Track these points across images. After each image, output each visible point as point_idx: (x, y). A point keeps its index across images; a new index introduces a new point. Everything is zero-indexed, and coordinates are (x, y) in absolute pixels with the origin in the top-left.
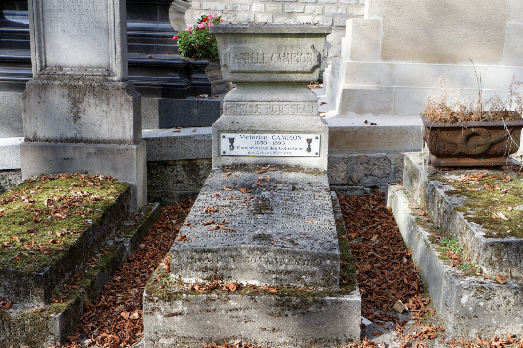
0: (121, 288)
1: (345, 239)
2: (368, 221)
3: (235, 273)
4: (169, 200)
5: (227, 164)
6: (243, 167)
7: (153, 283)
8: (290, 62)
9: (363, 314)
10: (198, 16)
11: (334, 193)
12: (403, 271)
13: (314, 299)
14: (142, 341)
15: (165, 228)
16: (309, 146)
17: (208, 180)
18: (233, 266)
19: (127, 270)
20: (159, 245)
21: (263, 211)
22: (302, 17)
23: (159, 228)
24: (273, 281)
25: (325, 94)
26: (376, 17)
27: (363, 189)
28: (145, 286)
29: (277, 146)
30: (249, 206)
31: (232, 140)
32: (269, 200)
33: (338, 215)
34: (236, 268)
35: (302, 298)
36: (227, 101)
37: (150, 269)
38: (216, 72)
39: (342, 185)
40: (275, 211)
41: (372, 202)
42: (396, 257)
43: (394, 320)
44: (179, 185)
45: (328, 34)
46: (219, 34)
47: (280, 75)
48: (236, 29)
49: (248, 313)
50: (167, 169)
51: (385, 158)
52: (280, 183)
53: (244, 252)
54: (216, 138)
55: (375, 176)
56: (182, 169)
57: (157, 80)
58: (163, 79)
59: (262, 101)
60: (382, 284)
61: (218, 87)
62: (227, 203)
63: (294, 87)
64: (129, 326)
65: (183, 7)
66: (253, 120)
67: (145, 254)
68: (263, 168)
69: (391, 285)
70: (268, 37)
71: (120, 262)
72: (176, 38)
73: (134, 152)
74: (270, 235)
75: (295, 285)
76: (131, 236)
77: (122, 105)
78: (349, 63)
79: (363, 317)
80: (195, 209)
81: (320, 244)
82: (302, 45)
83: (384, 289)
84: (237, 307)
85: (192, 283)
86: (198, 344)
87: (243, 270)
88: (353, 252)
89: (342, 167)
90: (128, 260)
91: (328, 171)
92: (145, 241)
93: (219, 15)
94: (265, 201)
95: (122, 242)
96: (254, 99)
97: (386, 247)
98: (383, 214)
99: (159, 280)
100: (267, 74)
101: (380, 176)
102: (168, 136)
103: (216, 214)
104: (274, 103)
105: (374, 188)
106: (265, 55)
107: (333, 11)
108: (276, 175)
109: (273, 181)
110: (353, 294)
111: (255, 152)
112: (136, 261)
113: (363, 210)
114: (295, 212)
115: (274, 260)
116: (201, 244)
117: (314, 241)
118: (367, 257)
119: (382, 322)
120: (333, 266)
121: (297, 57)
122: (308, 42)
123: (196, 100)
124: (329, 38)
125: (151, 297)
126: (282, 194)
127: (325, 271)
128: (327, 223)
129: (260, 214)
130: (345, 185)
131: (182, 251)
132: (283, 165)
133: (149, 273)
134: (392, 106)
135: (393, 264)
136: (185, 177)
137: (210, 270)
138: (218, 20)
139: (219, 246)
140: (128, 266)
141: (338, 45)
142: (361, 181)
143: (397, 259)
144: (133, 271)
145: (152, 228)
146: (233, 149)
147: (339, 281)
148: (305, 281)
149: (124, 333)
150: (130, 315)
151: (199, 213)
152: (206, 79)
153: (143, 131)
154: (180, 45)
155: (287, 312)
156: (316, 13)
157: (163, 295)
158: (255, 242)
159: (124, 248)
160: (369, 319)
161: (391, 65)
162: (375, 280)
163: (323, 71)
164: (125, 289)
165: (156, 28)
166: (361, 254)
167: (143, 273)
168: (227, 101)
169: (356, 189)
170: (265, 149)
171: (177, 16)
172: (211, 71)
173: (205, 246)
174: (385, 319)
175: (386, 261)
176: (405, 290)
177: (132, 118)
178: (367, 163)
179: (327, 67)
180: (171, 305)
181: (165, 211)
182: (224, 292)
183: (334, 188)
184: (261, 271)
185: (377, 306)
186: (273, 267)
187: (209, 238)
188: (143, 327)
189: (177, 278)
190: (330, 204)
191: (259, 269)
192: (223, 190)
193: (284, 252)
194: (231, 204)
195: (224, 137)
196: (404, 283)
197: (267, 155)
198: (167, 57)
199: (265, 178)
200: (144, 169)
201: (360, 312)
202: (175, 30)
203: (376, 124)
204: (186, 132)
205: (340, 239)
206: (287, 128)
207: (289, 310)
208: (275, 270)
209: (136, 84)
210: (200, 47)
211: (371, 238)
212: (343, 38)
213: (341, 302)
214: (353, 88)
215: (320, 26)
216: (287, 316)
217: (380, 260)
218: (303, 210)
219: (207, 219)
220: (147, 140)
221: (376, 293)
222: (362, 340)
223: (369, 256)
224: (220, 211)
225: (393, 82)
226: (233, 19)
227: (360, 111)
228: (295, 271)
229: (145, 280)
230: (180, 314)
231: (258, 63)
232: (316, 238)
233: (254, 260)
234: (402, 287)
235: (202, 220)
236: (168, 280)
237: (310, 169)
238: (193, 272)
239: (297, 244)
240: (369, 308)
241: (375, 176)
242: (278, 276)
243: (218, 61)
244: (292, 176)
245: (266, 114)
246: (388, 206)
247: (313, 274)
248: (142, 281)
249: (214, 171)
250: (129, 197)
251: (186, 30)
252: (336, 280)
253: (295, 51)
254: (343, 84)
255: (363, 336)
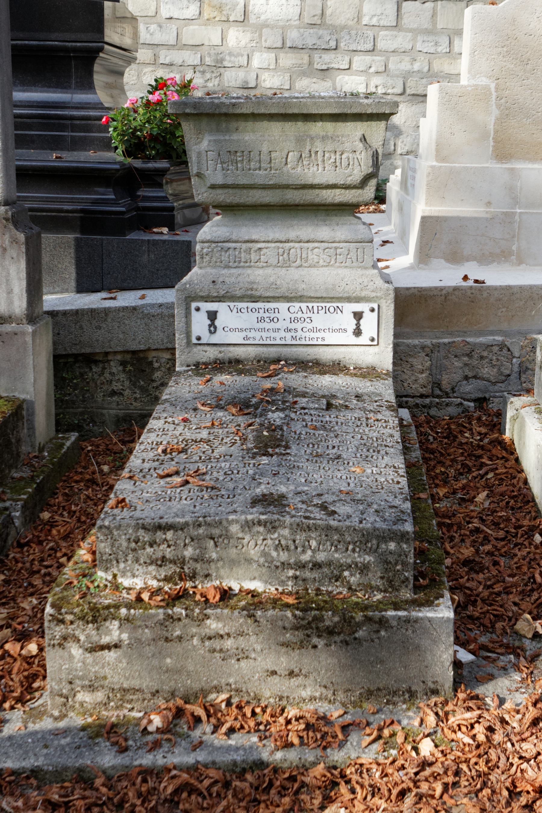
0: (6, 597)
1: (426, 500)
2: (470, 464)
3: (217, 569)
4: (96, 428)
5: (204, 360)
6: (233, 365)
7: (65, 589)
8: (320, 169)
9: (458, 641)
10: (149, 79)
11: (405, 413)
12: (535, 559)
13: (365, 616)
14: (44, 697)
15: (88, 480)
16: (358, 325)
17: (167, 391)
18: (214, 556)
19: (17, 562)
20: (78, 514)
21: (270, 450)
22: (347, 77)
23: (77, 482)
24: (290, 583)
25: (390, 223)
26: (483, 81)
27: (461, 404)
28: (48, 592)
29: (299, 326)
30: (244, 440)
31: (212, 316)
32: (281, 429)
33: (414, 455)
34: (220, 559)
35: (344, 614)
36: (203, 242)
37: (61, 560)
38: (183, 184)
39: (422, 396)
40: (294, 450)
41: (478, 429)
42: (520, 532)
43: (516, 651)
44: (115, 398)
45: (393, 114)
46: (187, 116)
47: (301, 191)
48: (218, 106)
49: (242, 642)
50: (91, 369)
51: (502, 346)
52: (304, 395)
53: (234, 529)
54: (184, 312)
55: (484, 379)
56: (121, 368)
57: (72, 201)
58: (82, 199)
59: (268, 242)
60: (495, 584)
61: (187, 212)
62: (204, 434)
63: (328, 215)
64: (19, 669)
65: (121, 63)
66: (252, 278)
67: (50, 531)
68: (272, 367)
69: (511, 587)
70: (278, 121)
71: (4, 547)
72: (107, 121)
73: (29, 339)
74: (282, 496)
75: (330, 589)
76: (25, 497)
77: (5, 250)
78: (432, 167)
79: (457, 648)
80: (142, 447)
81: (377, 511)
82: (342, 137)
83: (499, 594)
84: (222, 632)
85: (138, 587)
86: (149, 701)
87: (233, 563)
88: (440, 525)
89: (420, 362)
90: (18, 542)
91: (394, 371)
92: (51, 506)
93: (188, 78)
94: (274, 430)
95: (6, 509)
96: (254, 237)
97: (503, 514)
98: (497, 451)
99: (75, 582)
100: (277, 191)
101: (492, 378)
102: (94, 306)
103: (183, 456)
104: (292, 244)
105: (481, 402)
106: (273, 155)
107: (405, 66)
108: (296, 380)
109: (290, 393)
110: (438, 605)
111: (257, 337)
112: (33, 545)
113: (461, 444)
114: (331, 451)
115: (290, 542)
116: (153, 515)
117: (365, 506)
118: (468, 533)
119: (493, 655)
120: (402, 554)
121: (333, 157)
122: (354, 130)
123: (146, 238)
124: (396, 119)
125: (61, 614)
126: (306, 417)
127: (387, 562)
128: (391, 471)
129: (264, 455)
130: (427, 397)
131: (119, 527)
132: (308, 362)
133: (58, 568)
134: (514, 248)
135: (516, 545)
136: (127, 383)
137: (171, 562)
138: (186, 86)
139: (188, 518)
140: (18, 555)
141: (414, 131)
142: (456, 389)
143: (522, 536)
144: (28, 565)
145: (65, 481)
146: (215, 332)
147: (412, 582)
148: (348, 582)
149: (11, 683)
150: (22, 648)
151: (151, 455)
152: (164, 199)
153: (45, 297)
154: (115, 134)
155: (315, 640)
156: (372, 70)
157: (82, 611)
158: (255, 509)
159: (10, 520)
160: (470, 651)
161: (512, 169)
162: (481, 576)
163: (386, 181)
164: (14, 599)
165: (69, 103)
166: (455, 528)
167: (47, 567)
168: (203, 242)
169: (447, 405)
170: (275, 330)
171: (110, 79)
172: (175, 184)
173: (161, 518)
174: (499, 651)
175: (502, 539)
176: (537, 595)
177: (23, 275)
178: (468, 355)
179: (393, 173)
180: (98, 629)
181: (90, 448)
182: (197, 603)
183: (407, 402)
184: (266, 564)
185: (484, 626)
186: (290, 556)
187: (169, 503)
188: (45, 670)
189: (110, 578)
190: (397, 436)
191: (262, 560)
192: (195, 409)
193: (308, 527)
194: (212, 438)
195: (198, 309)
196: (535, 582)
197: (278, 342)
198: (90, 157)
199: (275, 386)
200: (48, 371)
201: (452, 639)
202: (106, 105)
203: (484, 283)
204: (127, 299)
205: (414, 499)
206: (316, 291)
207: (319, 636)
208: (292, 561)
209: (31, 210)
210: (153, 138)
211: (474, 497)
212: (422, 120)
213: (417, 620)
214: (440, 214)
215: (377, 100)
216: (315, 647)
217: (491, 538)
218: (345, 448)
219: (166, 466)
220: (52, 314)
221: (483, 601)
222: (455, 690)
223: (471, 532)
224: (189, 451)
225: (515, 201)
226: (216, 83)
227: (455, 257)
228: (329, 564)
229: (50, 581)
230: (116, 646)
231: (260, 169)
232: (369, 500)
233: (252, 543)
234: (532, 590)
235: (155, 469)
236: (92, 582)
237: (360, 369)
238: (140, 568)
239: (334, 512)
240: (470, 630)
241: (484, 379)
242: (298, 573)
243: (186, 163)
244: (326, 382)
245: (276, 266)
246: (508, 435)
247: (364, 569)
248: (44, 582)
249: (179, 373)
250: (20, 424)
251: (125, 106)
252: (407, 579)
253: (330, 147)
254: (422, 208)
255: (457, 683)
